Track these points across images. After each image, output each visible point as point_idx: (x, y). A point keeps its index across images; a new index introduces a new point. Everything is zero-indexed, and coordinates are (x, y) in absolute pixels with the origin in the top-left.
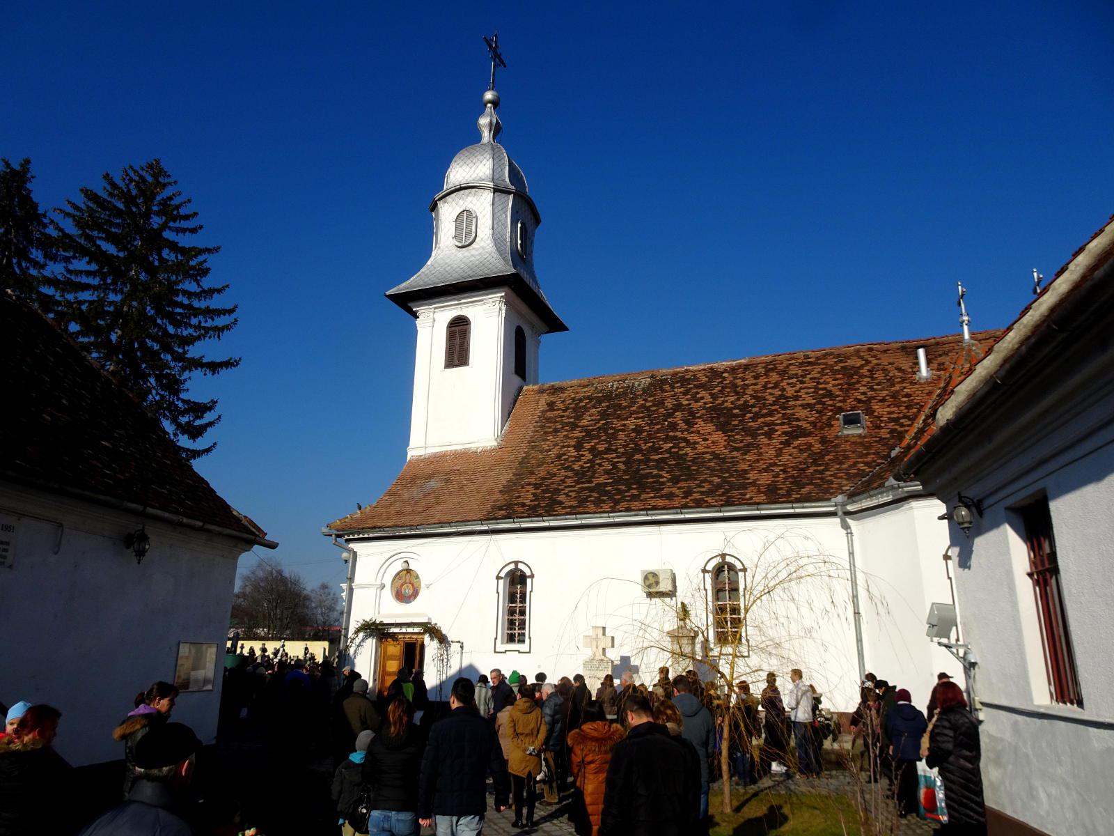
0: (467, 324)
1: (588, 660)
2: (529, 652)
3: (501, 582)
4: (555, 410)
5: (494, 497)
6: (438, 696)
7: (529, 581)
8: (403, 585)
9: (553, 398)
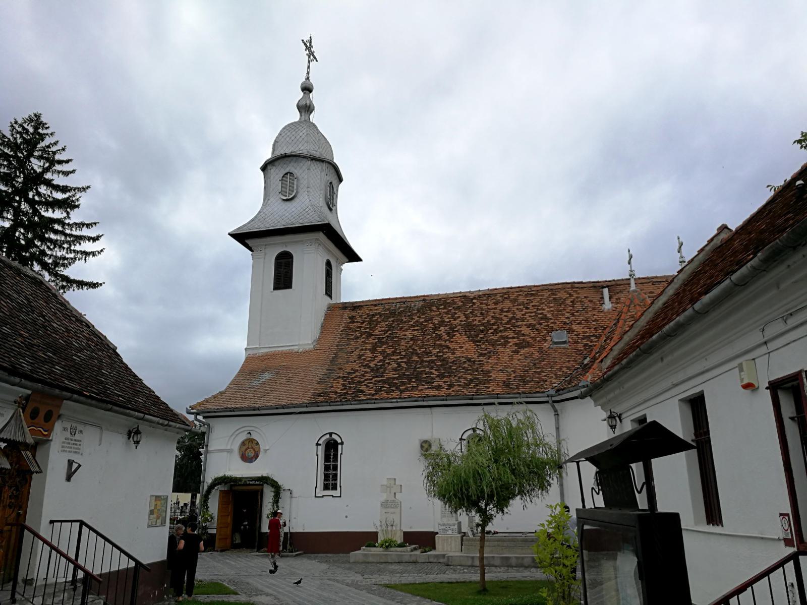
2: (340, 496)
3: (320, 447)
7: (340, 447)
8: (246, 449)
9: (354, 314)
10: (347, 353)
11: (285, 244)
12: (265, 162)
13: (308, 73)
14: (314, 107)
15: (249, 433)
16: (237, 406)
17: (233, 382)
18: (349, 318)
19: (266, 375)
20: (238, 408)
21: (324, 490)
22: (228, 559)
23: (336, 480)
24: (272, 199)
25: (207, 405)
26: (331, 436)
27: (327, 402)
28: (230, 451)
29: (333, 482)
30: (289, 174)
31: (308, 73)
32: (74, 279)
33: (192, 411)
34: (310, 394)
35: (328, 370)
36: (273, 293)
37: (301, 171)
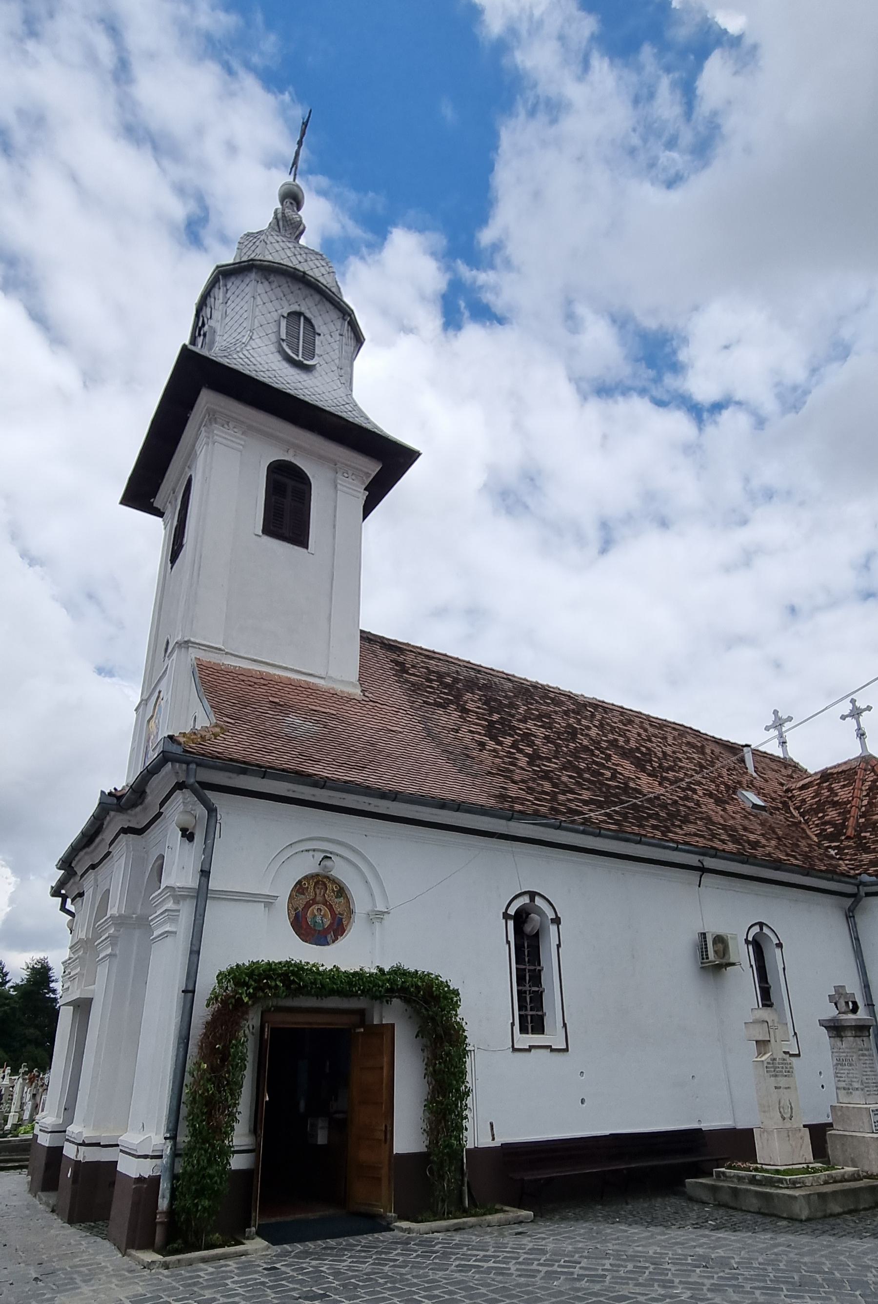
8: (308, 906)
26: (761, 929)
28: (269, 901)
32: (255, 965)
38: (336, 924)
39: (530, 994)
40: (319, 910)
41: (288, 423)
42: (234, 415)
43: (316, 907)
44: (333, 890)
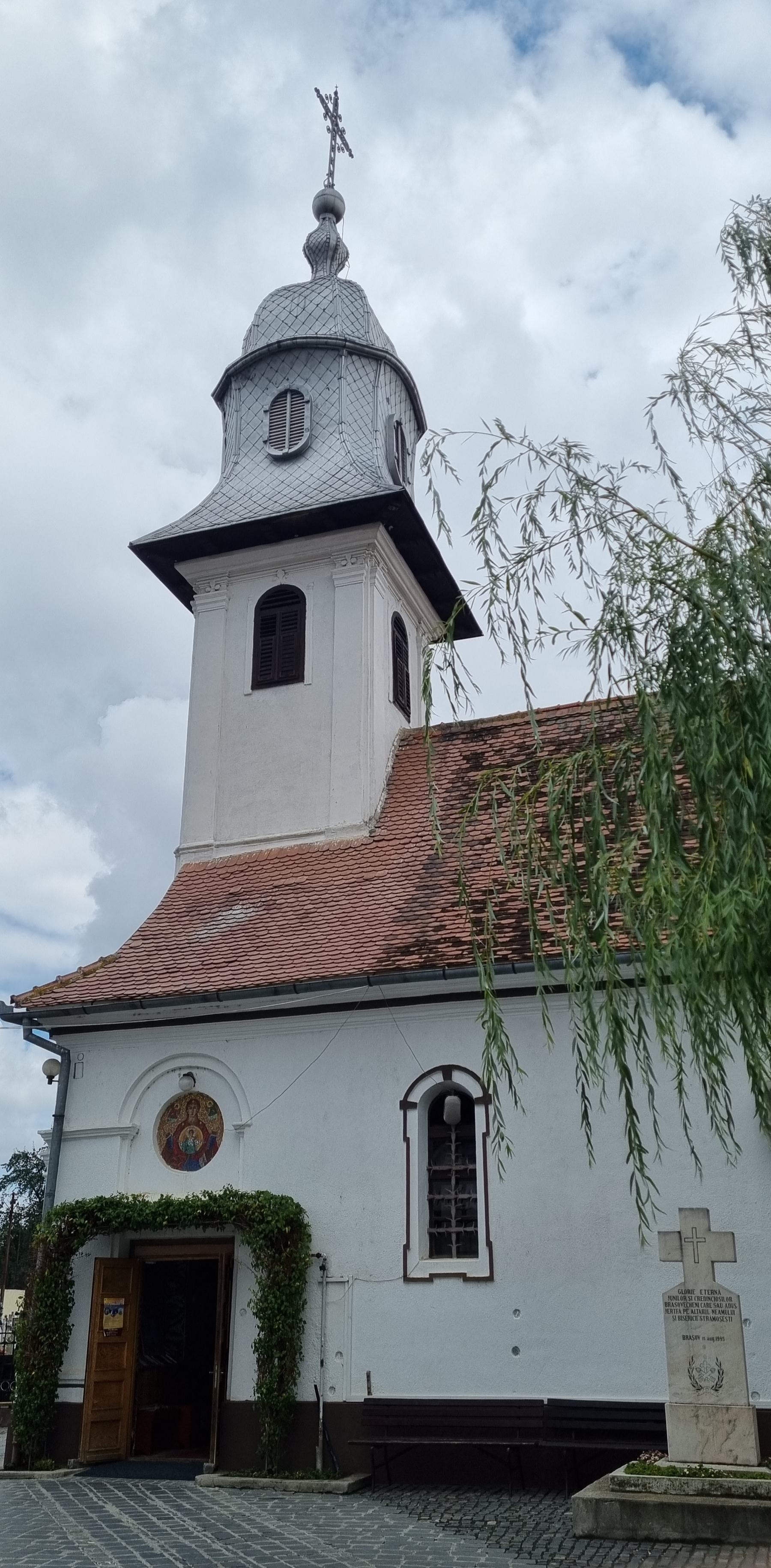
0: (299, 602)
1: (676, 1294)
2: (490, 1279)
3: (414, 1116)
4: (484, 768)
5: (385, 931)
6: (63, 1383)
7: (479, 1112)
8: (180, 1128)
9: (476, 747)
10: (470, 844)
11: (285, 566)
12: (227, 370)
13: (331, 174)
14: (348, 254)
15: (189, 1075)
16: (152, 991)
17: (142, 934)
18: (465, 758)
19: (238, 913)
20: (157, 996)
21: (431, 1256)
22: (117, 1502)
23: (474, 1221)
24: (244, 461)
25: (61, 993)
27: (434, 966)
28: (129, 1135)
29: (461, 1229)
30: (289, 396)
31: (331, 174)
32: (100, 1199)
33: (16, 1010)
34: (375, 950)
35: (418, 888)
36: (249, 698)
37: (321, 386)
38: (208, 1144)
39: (456, 1203)
40: (192, 1131)
41: (262, 546)
42: (211, 573)
43: (188, 1129)
44: (206, 1108)
